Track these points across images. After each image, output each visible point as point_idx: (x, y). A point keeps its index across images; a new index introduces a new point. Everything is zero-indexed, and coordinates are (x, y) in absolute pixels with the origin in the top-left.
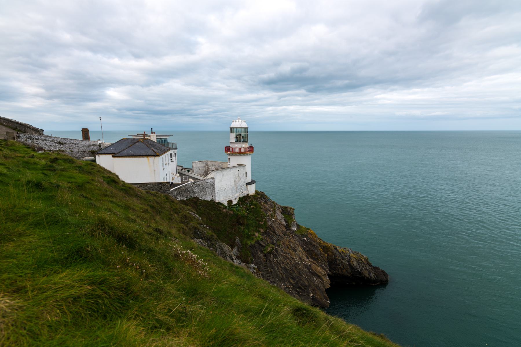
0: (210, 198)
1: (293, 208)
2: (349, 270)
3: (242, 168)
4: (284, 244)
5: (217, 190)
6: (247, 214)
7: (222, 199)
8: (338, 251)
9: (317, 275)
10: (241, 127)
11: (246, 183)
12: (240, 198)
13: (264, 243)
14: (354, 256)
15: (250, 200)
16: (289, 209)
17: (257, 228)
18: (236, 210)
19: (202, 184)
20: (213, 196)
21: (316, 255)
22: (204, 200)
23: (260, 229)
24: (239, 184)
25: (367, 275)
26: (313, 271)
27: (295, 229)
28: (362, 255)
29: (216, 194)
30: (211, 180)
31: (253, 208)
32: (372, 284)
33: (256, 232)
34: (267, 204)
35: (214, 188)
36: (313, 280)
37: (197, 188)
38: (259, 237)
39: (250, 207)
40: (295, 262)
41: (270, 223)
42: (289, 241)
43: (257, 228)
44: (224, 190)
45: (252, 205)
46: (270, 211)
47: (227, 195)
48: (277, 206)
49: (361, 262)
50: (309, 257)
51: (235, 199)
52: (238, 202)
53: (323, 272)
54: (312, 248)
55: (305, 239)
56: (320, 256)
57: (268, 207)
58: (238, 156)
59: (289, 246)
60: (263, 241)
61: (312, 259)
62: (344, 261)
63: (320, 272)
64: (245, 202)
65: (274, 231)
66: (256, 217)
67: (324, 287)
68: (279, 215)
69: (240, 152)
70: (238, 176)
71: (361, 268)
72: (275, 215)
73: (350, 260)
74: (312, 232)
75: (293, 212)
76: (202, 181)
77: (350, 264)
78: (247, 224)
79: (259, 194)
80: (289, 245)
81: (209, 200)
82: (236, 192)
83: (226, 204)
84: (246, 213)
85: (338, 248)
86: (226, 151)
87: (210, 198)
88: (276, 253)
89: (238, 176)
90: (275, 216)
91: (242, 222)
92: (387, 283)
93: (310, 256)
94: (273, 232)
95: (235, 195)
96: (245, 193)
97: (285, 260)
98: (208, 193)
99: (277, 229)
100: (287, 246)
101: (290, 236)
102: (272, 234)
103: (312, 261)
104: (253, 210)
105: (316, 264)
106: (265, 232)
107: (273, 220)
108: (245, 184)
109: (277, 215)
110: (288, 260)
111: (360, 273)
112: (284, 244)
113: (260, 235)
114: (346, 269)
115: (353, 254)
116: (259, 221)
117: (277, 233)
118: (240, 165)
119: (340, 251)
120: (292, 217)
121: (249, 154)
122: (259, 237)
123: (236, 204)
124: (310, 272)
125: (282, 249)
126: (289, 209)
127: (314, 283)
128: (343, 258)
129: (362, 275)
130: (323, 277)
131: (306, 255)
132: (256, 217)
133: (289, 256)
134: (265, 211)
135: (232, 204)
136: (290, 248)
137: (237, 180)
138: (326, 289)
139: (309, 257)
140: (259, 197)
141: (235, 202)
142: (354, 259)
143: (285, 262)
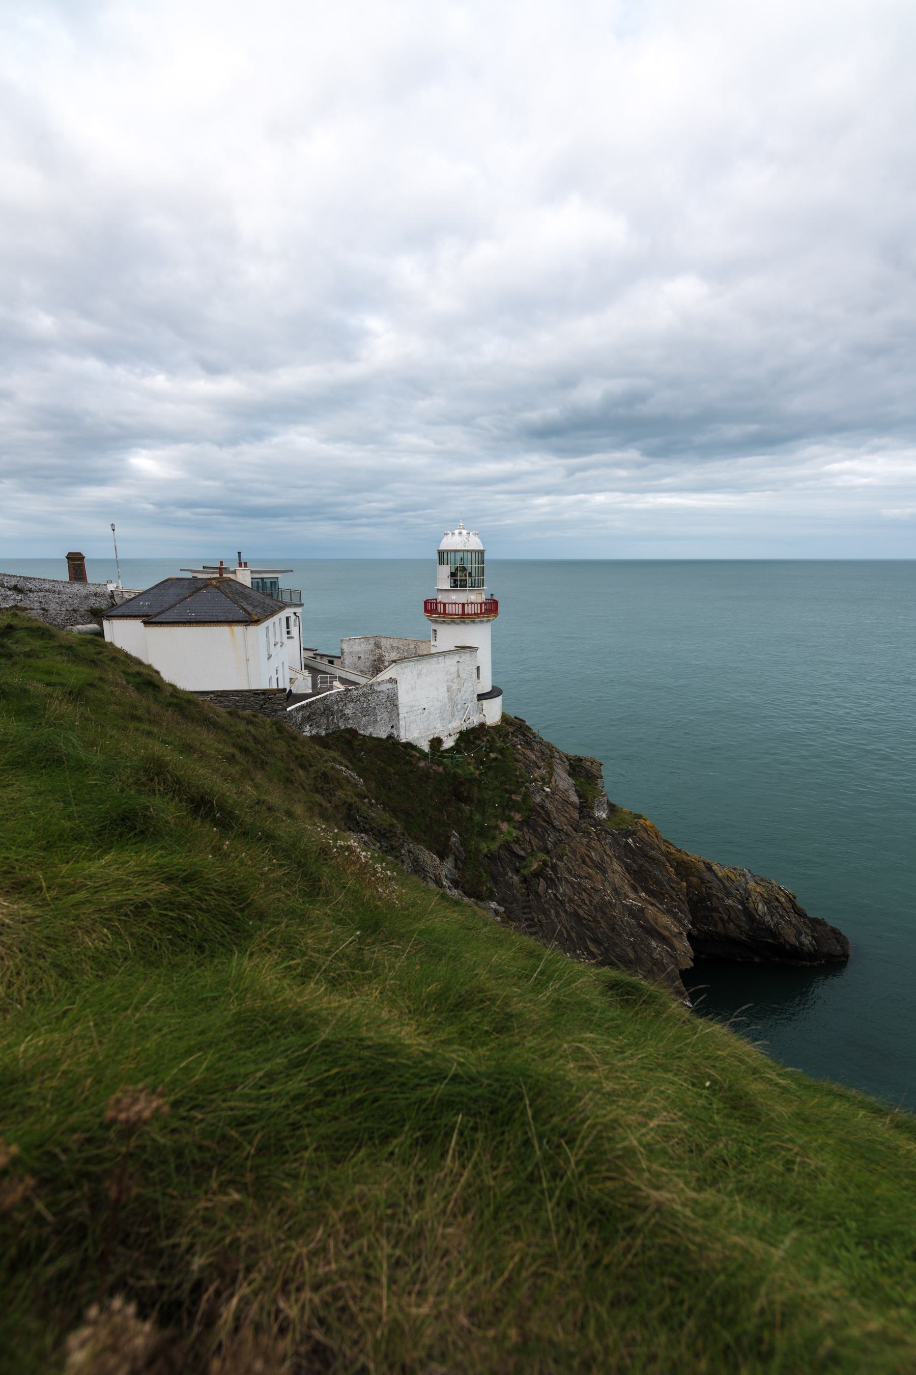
0: (385, 731)
4: (574, 852)
5: (402, 710)
7: (416, 735)
8: (716, 875)
10: (466, 549)
12: (461, 733)
17: (504, 810)
20: (392, 727)
21: (658, 882)
23: (512, 814)
24: (459, 696)
25: (793, 940)
27: (604, 816)
28: (780, 888)
29: (402, 723)
30: (389, 686)
31: (495, 759)
32: (804, 963)
33: (503, 821)
34: (532, 750)
35: (396, 705)
37: (352, 704)
38: (510, 833)
39: (487, 756)
40: (602, 899)
43: (504, 810)
44: (421, 711)
45: (493, 752)
46: (539, 768)
47: (429, 725)
48: (556, 755)
49: (777, 904)
50: (639, 889)
51: (450, 735)
53: (675, 926)
56: (668, 887)
59: (587, 859)
60: (520, 845)
61: (646, 893)
62: (730, 902)
64: (474, 743)
65: (550, 818)
66: (503, 783)
67: (677, 965)
69: (463, 613)
70: (458, 676)
71: (775, 920)
72: (551, 778)
73: (747, 899)
75: (600, 770)
79: (511, 724)
81: (384, 736)
83: (426, 748)
84: (478, 772)
85: (715, 867)
86: (426, 610)
87: (385, 731)
88: (553, 876)
89: (458, 676)
90: (553, 780)
94: (545, 821)
95: (450, 726)
96: (475, 720)
97: (575, 895)
98: (381, 719)
100: (582, 857)
102: (543, 827)
103: (647, 898)
104: (494, 764)
106: (525, 822)
107: (548, 790)
108: (475, 696)
110: (584, 894)
111: (773, 934)
113: (511, 829)
116: (511, 793)
117: (558, 823)
119: (720, 874)
124: (641, 926)
125: (569, 864)
127: (650, 954)
128: (729, 894)
130: (674, 940)
131: (632, 882)
132: (503, 783)
133: (587, 884)
134: (527, 766)
135: (442, 749)
137: (455, 687)
138: (681, 971)
139: (639, 889)
141: (448, 743)
142: (759, 897)
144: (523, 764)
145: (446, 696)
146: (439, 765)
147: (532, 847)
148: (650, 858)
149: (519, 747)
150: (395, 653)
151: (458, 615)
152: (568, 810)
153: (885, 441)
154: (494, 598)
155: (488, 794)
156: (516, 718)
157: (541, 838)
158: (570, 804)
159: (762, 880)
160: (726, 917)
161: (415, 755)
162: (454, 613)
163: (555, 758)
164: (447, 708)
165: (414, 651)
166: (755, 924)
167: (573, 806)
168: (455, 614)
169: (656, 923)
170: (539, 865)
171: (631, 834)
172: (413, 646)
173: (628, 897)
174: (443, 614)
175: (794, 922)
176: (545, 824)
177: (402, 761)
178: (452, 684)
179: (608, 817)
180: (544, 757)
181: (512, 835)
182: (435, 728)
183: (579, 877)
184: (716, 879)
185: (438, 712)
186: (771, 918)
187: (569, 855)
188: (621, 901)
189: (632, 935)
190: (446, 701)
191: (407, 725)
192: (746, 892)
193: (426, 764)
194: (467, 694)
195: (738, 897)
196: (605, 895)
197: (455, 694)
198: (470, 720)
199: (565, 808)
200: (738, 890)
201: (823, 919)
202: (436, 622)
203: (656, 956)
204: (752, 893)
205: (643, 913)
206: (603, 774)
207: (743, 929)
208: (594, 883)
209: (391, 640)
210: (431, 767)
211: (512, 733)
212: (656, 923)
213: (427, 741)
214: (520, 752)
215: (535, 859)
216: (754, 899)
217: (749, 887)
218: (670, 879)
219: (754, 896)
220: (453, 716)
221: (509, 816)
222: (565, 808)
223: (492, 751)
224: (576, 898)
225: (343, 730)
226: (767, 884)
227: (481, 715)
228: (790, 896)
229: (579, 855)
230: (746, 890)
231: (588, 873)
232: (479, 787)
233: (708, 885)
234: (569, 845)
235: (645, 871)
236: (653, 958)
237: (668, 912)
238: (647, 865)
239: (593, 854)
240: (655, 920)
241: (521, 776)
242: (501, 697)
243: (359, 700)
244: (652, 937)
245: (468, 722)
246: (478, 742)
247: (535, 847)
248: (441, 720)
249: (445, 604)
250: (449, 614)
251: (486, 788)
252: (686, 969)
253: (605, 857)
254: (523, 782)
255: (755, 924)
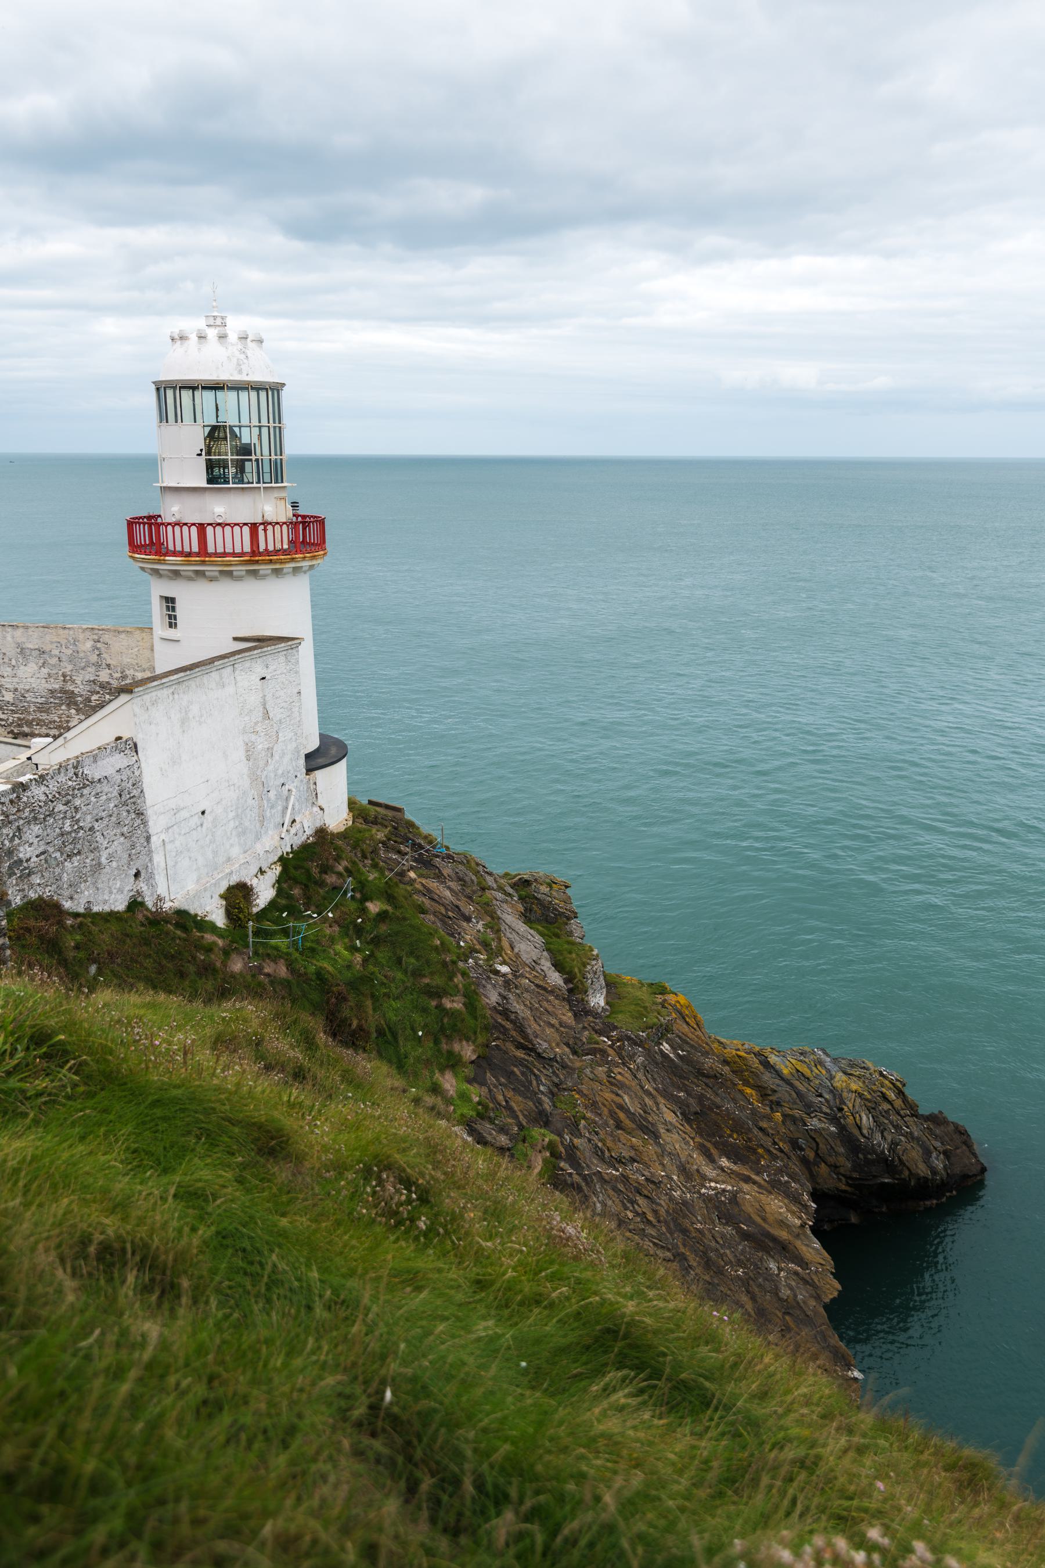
0: (120, 891)
1: (560, 879)
2: (841, 1160)
3: (282, 659)
4: (594, 1106)
5: (156, 824)
6: (365, 960)
7: (191, 886)
8: (779, 1074)
9: (775, 1239)
10: (244, 378)
11: (308, 757)
12: (281, 859)
13: (503, 1130)
14: (854, 1087)
15: (345, 863)
16: (544, 889)
17: (437, 1042)
18: (295, 944)
19: (65, 796)
20: (137, 875)
21: (738, 1127)
22: (89, 914)
23: (456, 1047)
24: (271, 768)
25: (922, 1170)
26: (754, 1222)
27: (602, 1003)
28: (881, 1074)
29: (158, 859)
30: (119, 761)
31: (382, 916)
32: (928, 1203)
33: (442, 1071)
34: (439, 876)
35: (140, 814)
36: (769, 1277)
37: (36, 829)
38: (464, 1096)
39: (364, 911)
40: (672, 1199)
41: (493, 997)
42: (615, 1085)
43: (437, 1042)
44: (196, 820)
45: (371, 899)
46: (468, 919)
47: (215, 853)
48: (490, 881)
49: (886, 1106)
50: (714, 1151)
51: (262, 872)
52: (280, 892)
53: (793, 1213)
54: (709, 1094)
55: (666, 1047)
56: (755, 1131)
57: (448, 893)
58: (239, 578)
59: (622, 1115)
60: (491, 1121)
61: (729, 1158)
62: (815, 1122)
63: (782, 1224)
64: (321, 884)
65: (526, 1037)
66: (417, 974)
67: (818, 1298)
68: (522, 937)
69: (255, 552)
70: (266, 715)
71: (889, 1138)
72: (500, 940)
73: (841, 1110)
74: (682, 999)
75: (568, 900)
76: (62, 778)
77: (842, 1128)
78: (380, 1033)
79: (375, 822)
80: (621, 1107)
81: (119, 904)
82: (262, 823)
83: (219, 918)
84: (358, 958)
85: (773, 1059)
86: (134, 547)
87: (120, 891)
88: (577, 1178)
89: (266, 715)
90: (505, 944)
91: (355, 1023)
92: (981, 1184)
93: (716, 1145)
94: (520, 1046)
95: (259, 848)
96: (307, 826)
97: (626, 1209)
98: (111, 858)
99: (535, 1026)
100: (612, 1114)
101: (603, 1052)
102: (520, 1063)
103: (735, 1168)
104: (383, 928)
105: (755, 1183)
106: (483, 1062)
107: (504, 969)
108: (302, 761)
109: (513, 936)
110: (641, 1200)
111: (889, 1164)
112: (594, 1106)
113: (465, 1086)
114: (831, 1160)
115: (845, 1073)
116: (437, 993)
117: (545, 1045)
118: (262, 641)
119: (785, 1071)
120: (570, 934)
121: (305, 564)
122: (464, 1096)
123: (272, 904)
124: (745, 1236)
125: (595, 1138)
126: (544, 889)
127: (776, 1292)
128: (809, 1109)
129: (901, 1172)
130: (798, 1243)
131: (698, 1139)
132: (417, 974)
133: (636, 1174)
134: (444, 919)
135: (255, 910)
136: (627, 1123)
137: (261, 745)
138: (826, 1307)
139: (714, 1151)
140: (380, 836)
141: (265, 894)
142: (858, 1100)
143: (630, 1215)
144: (435, 913)
145: (245, 771)
146: (275, 960)
147: (516, 1117)
148: (708, 1076)
149: (412, 874)
150: (32, 667)
151: (242, 554)
152: (550, 1009)
153: (711, 239)
154: (301, 511)
155: (394, 1010)
156: (370, 802)
157: (527, 1091)
158: (552, 992)
159: (852, 1065)
160: (811, 1155)
161: (215, 943)
162: (229, 550)
163: (490, 888)
164: (250, 801)
165: (94, 658)
166: (861, 1156)
167: (557, 997)
168: (234, 554)
169: (764, 1219)
170: (545, 1160)
171: (663, 1032)
172: (89, 644)
173: (704, 1178)
174: (198, 554)
175: (916, 1134)
176: (520, 1054)
177: (192, 969)
178: (253, 737)
179: (607, 1003)
180: (468, 891)
181: (470, 1100)
182: (229, 859)
183: (620, 1162)
184: (781, 1083)
185: (232, 815)
186: (883, 1136)
187: (589, 1115)
188: (699, 1192)
189: (740, 1263)
190: (246, 783)
191: (170, 863)
192: (834, 1096)
193: (245, 964)
194: (286, 759)
195: (825, 1109)
196: (671, 1189)
197: (261, 763)
198: (297, 825)
199: (545, 1004)
200: (820, 1096)
201: (941, 1112)
202: (176, 574)
203: (785, 1293)
204: (845, 1094)
205: (737, 1204)
206: (575, 905)
207: (842, 1170)
208: (648, 1167)
209: (19, 633)
210: (260, 968)
211: (383, 843)
212: (764, 1219)
213: (216, 897)
214: (418, 886)
215: (532, 1146)
216: (850, 1106)
217: (837, 1084)
218: (754, 1112)
219: (851, 1102)
220: (262, 820)
221: (450, 1053)
222: (545, 1004)
223: (366, 898)
224: (630, 1215)
225: (20, 909)
226: (862, 1072)
227: (316, 809)
228: (898, 1084)
229: (606, 1111)
230: (833, 1091)
231: (632, 1147)
232: (373, 996)
233: (773, 1098)
234: (580, 1092)
235: (711, 1109)
236: (780, 1299)
237: (774, 1186)
238: (709, 1094)
239: (626, 1098)
240: (762, 1209)
241: (444, 948)
242: (344, 762)
243: (51, 814)
244: (767, 1250)
245: (293, 831)
246: (331, 879)
247: (521, 1117)
248: (239, 835)
249: (202, 528)
250: (216, 554)
251: (387, 995)
252: (833, 1300)
253: (647, 1100)
254: (454, 963)
255: (861, 1156)
